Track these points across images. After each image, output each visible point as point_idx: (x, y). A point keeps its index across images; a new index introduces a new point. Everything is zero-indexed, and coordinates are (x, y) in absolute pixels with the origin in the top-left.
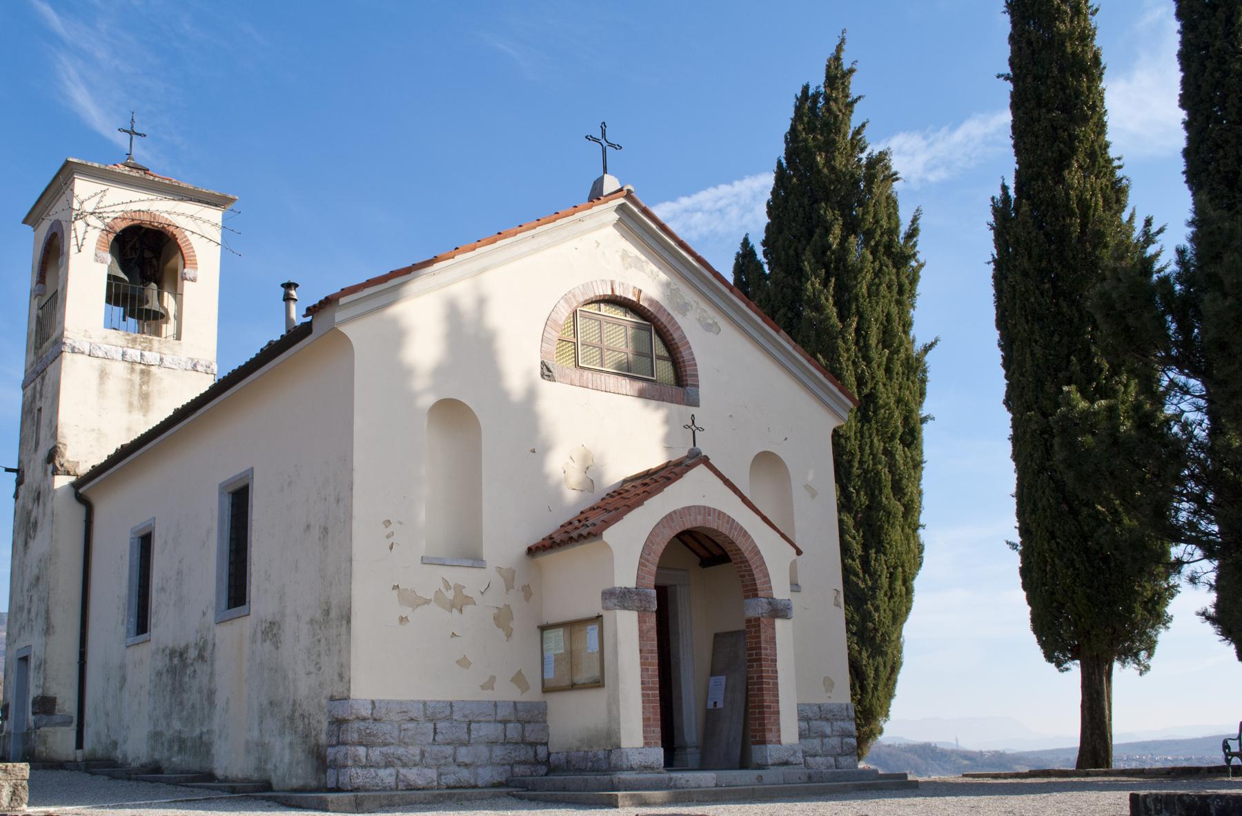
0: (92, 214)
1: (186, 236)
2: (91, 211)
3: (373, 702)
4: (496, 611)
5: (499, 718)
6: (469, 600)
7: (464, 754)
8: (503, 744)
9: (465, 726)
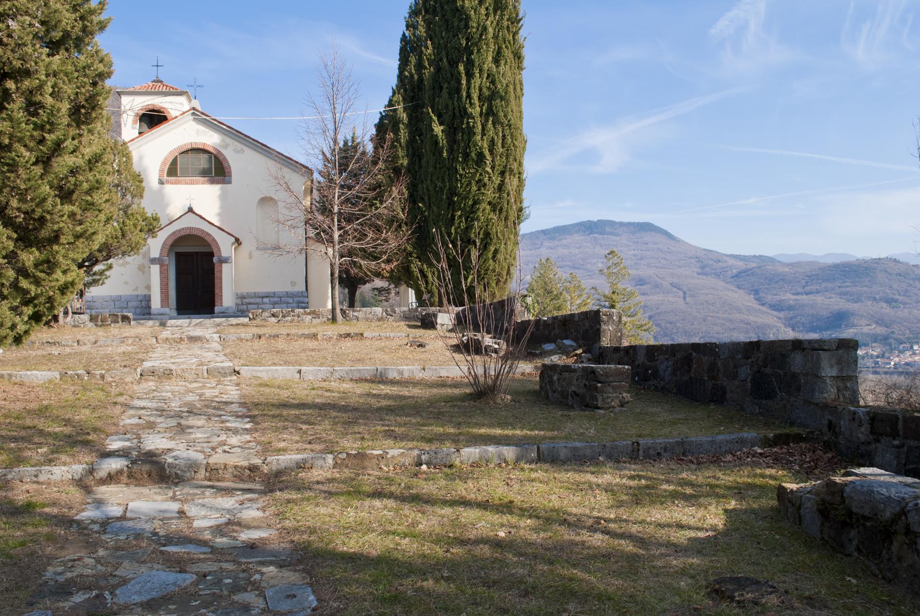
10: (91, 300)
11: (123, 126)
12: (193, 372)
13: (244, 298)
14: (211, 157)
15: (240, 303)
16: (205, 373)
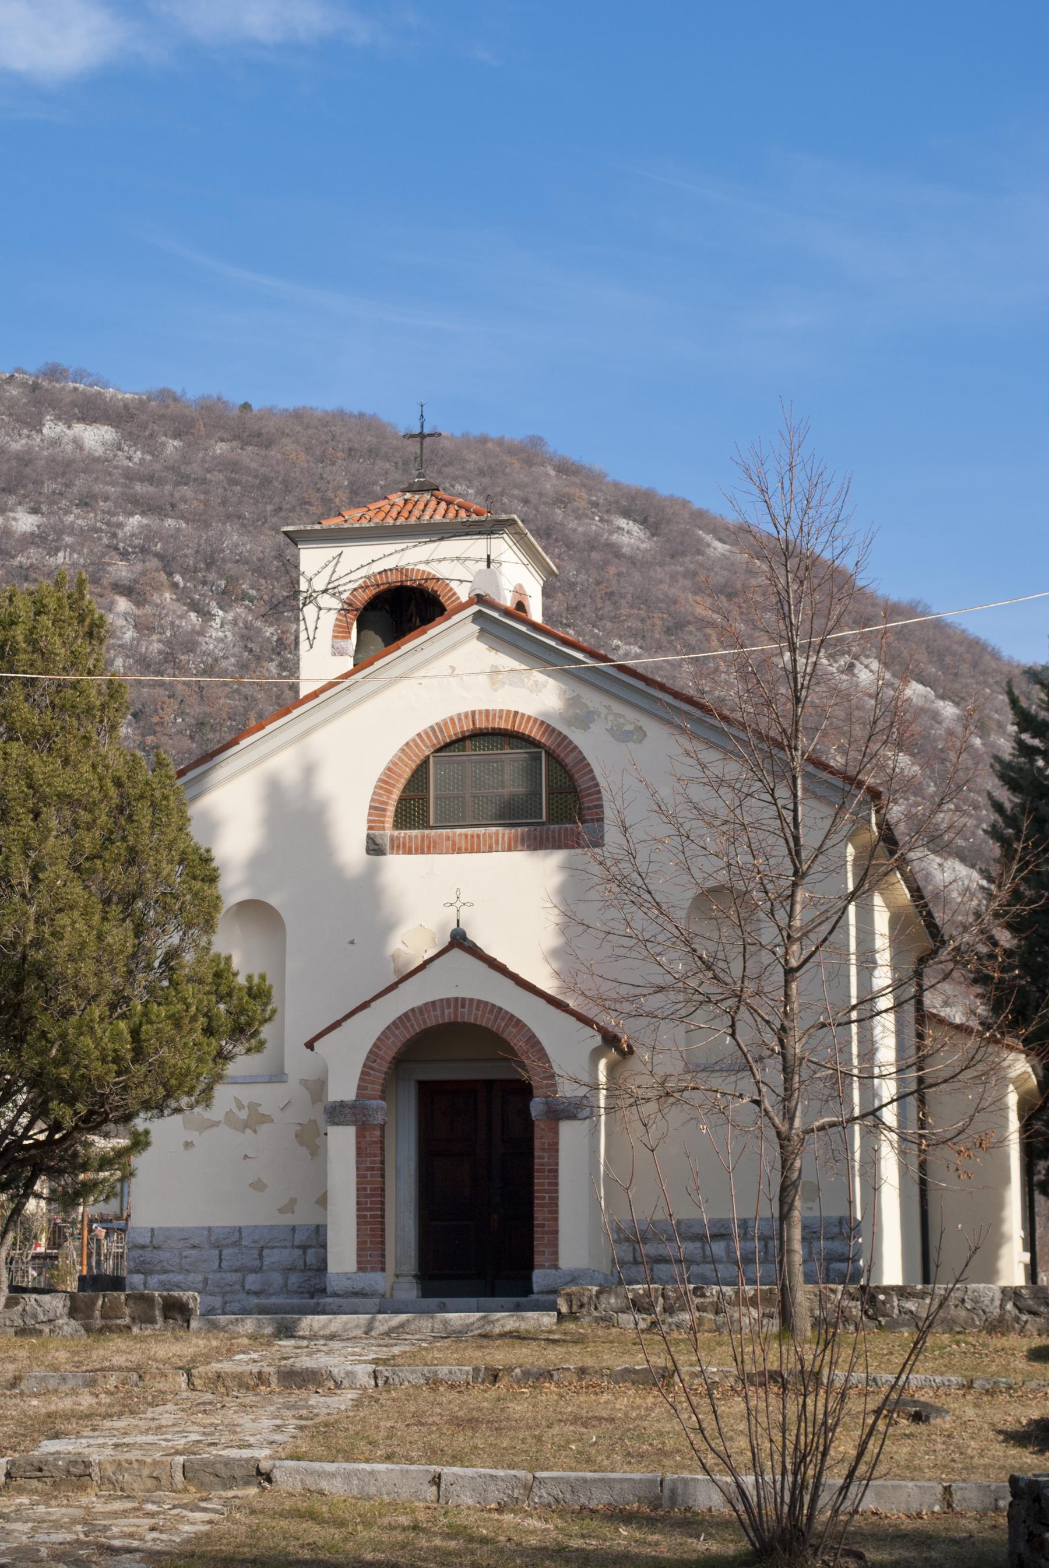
0: (325, 591)
1: (451, 589)
2: (323, 588)
3: (152, 1230)
4: (299, 1128)
5: (296, 1243)
6: (266, 1119)
7: (252, 1281)
8: (303, 1271)
9: (255, 1252)
10: (145, 1240)
11: (304, 645)
12: (146, 1472)
13: (645, 1240)
14: (537, 758)
15: (629, 1257)
16: (179, 1476)
